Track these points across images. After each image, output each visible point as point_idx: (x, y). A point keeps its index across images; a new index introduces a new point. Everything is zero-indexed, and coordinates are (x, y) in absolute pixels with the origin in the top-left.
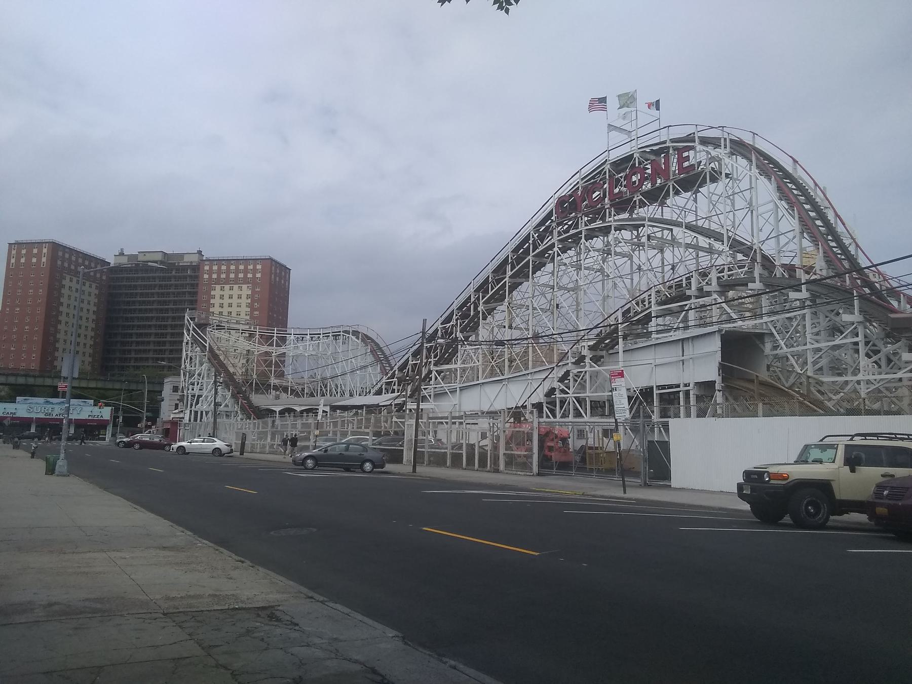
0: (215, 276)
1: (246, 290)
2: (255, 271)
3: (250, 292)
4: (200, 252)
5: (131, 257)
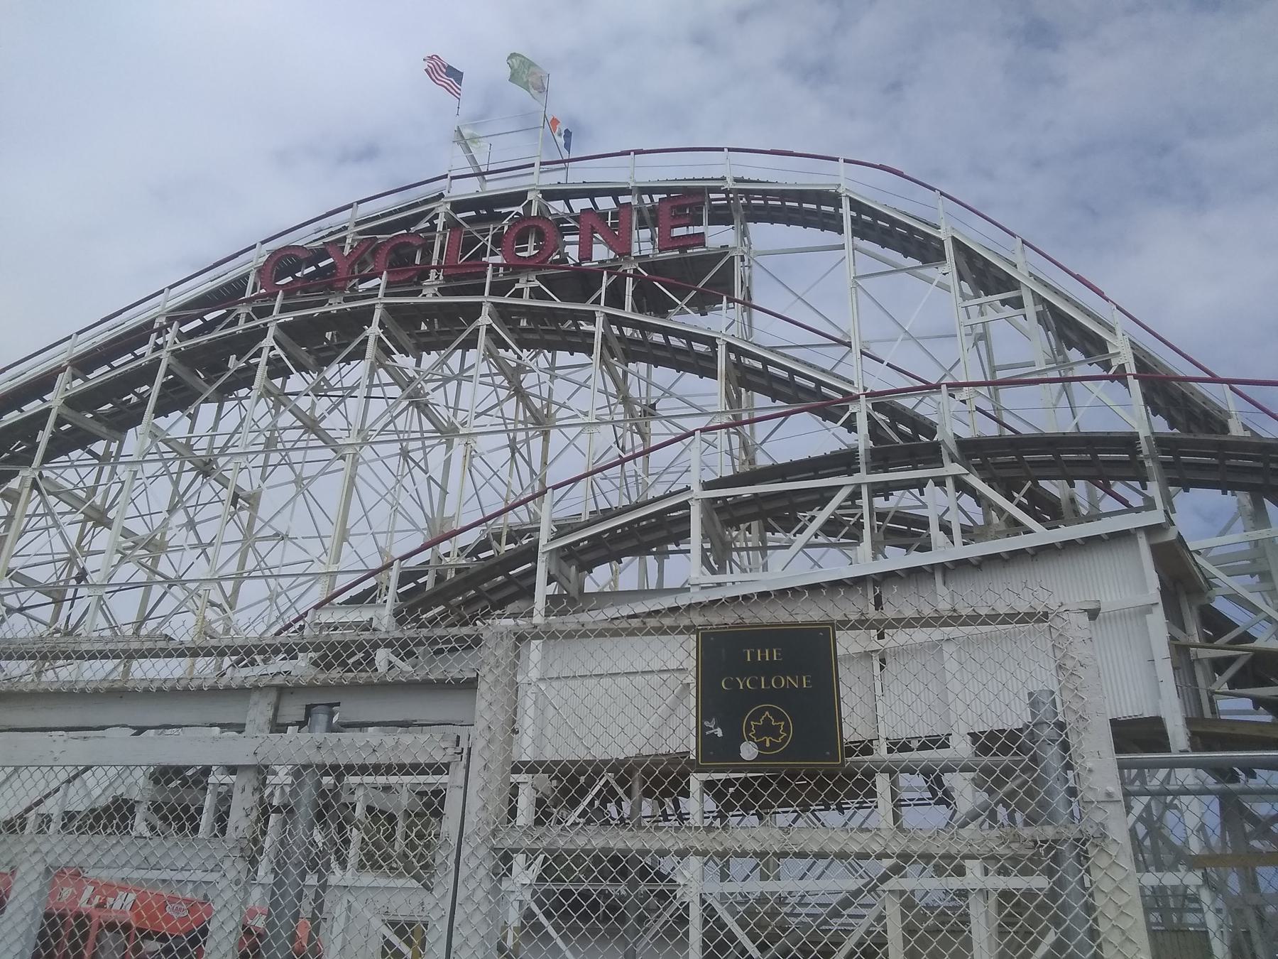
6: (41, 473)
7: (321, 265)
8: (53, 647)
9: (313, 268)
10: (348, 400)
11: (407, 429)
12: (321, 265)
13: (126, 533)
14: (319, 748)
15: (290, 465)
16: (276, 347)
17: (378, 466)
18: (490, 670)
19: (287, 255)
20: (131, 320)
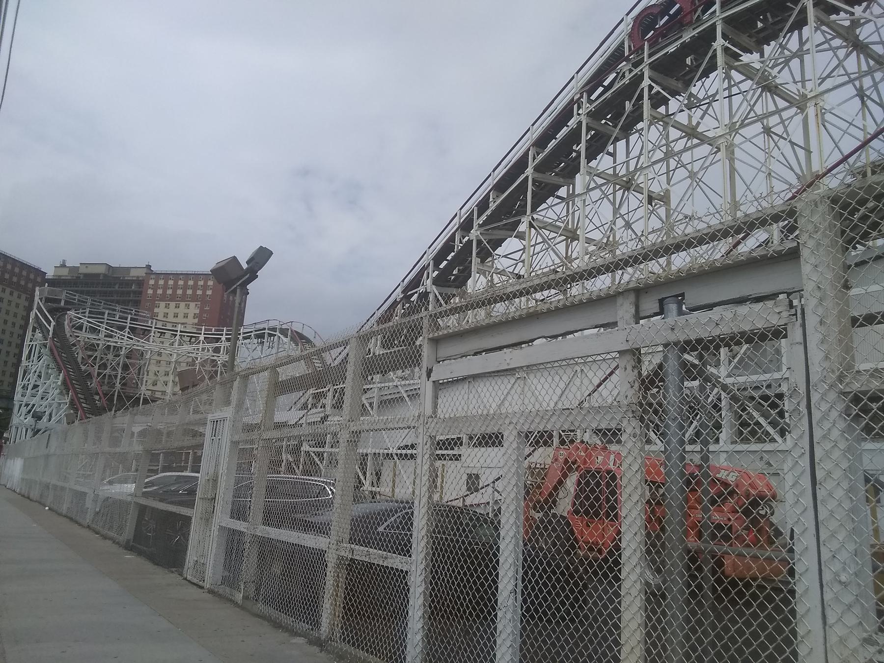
0: (160, 292)
1: (194, 309)
2: (205, 288)
3: (197, 311)
4: (149, 267)
5: (74, 269)
6: (532, 217)
7: (671, 12)
8: (493, 294)
9: (667, 18)
10: (713, 104)
11: (765, 112)
12: (671, 12)
13: (589, 241)
14: (673, 329)
15: (684, 166)
16: (653, 84)
17: (747, 146)
18: (810, 236)
19: (646, 15)
20: (560, 104)
